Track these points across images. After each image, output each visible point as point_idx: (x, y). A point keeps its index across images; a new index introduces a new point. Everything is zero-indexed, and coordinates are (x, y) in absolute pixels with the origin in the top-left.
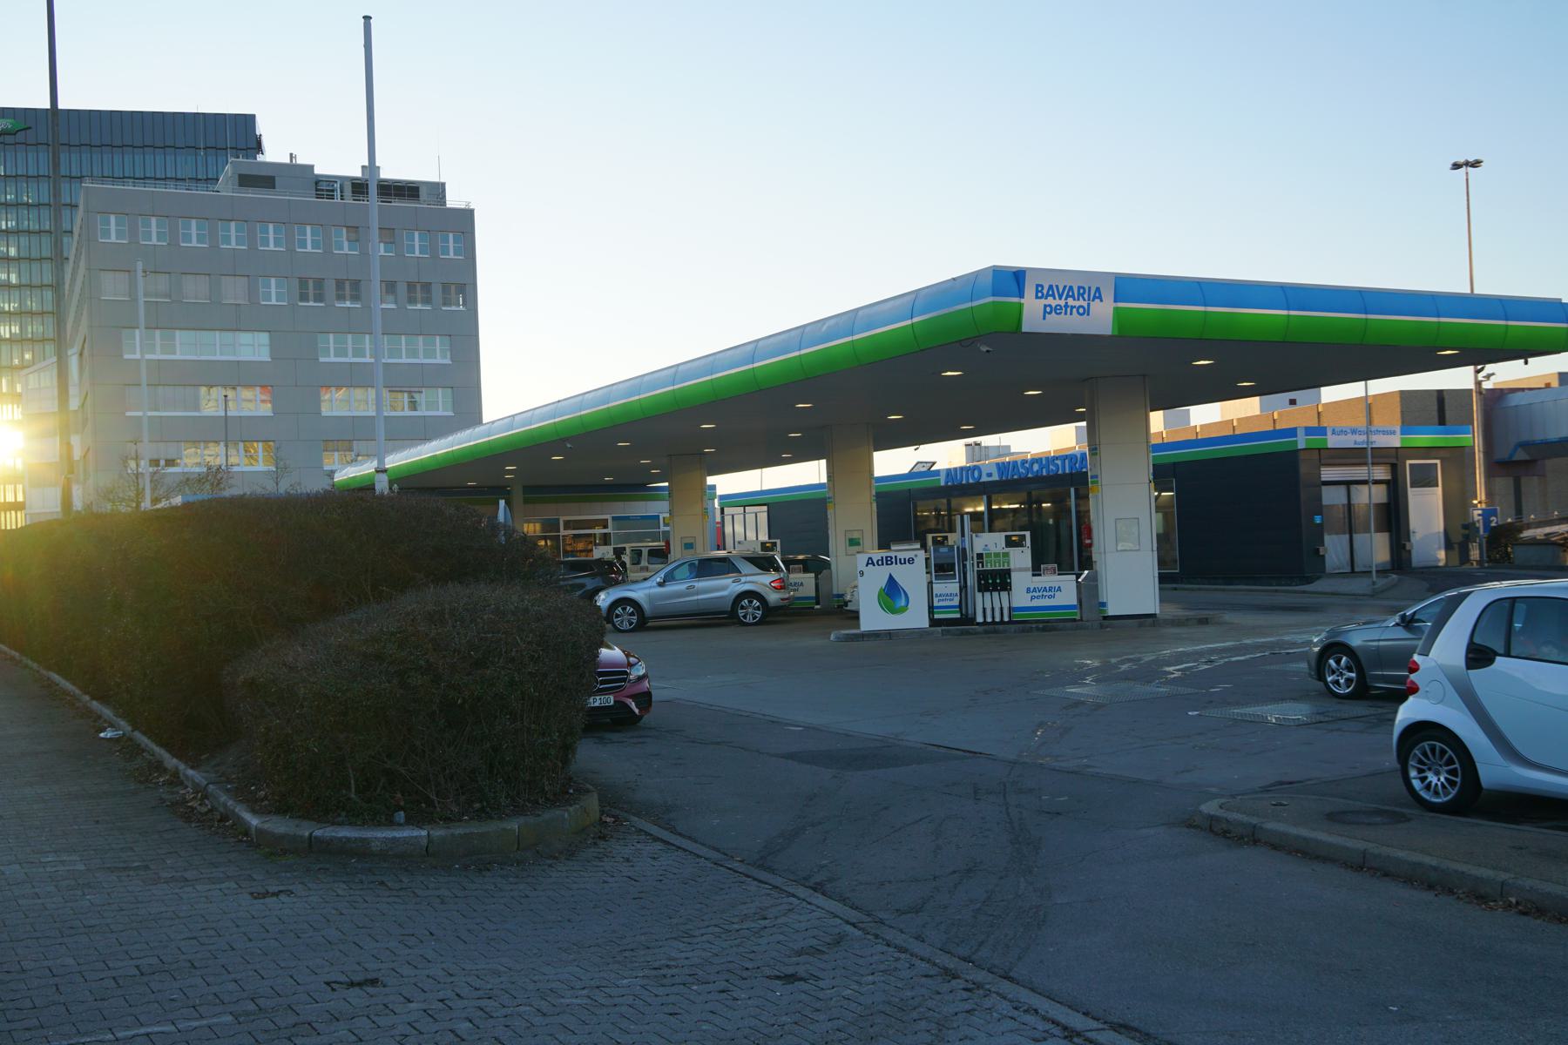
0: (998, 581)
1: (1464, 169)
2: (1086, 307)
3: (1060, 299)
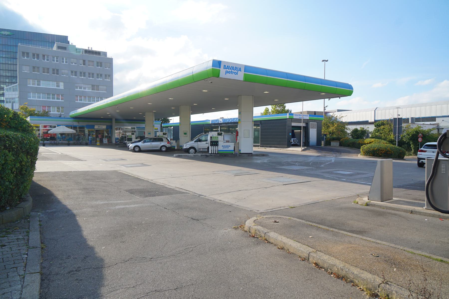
0: (215, 143)
1: (324, 62)
2: (237, 72)
3: (230, 69)
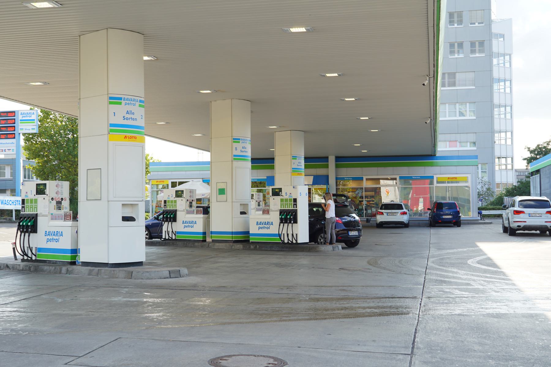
2: (269, 227)
